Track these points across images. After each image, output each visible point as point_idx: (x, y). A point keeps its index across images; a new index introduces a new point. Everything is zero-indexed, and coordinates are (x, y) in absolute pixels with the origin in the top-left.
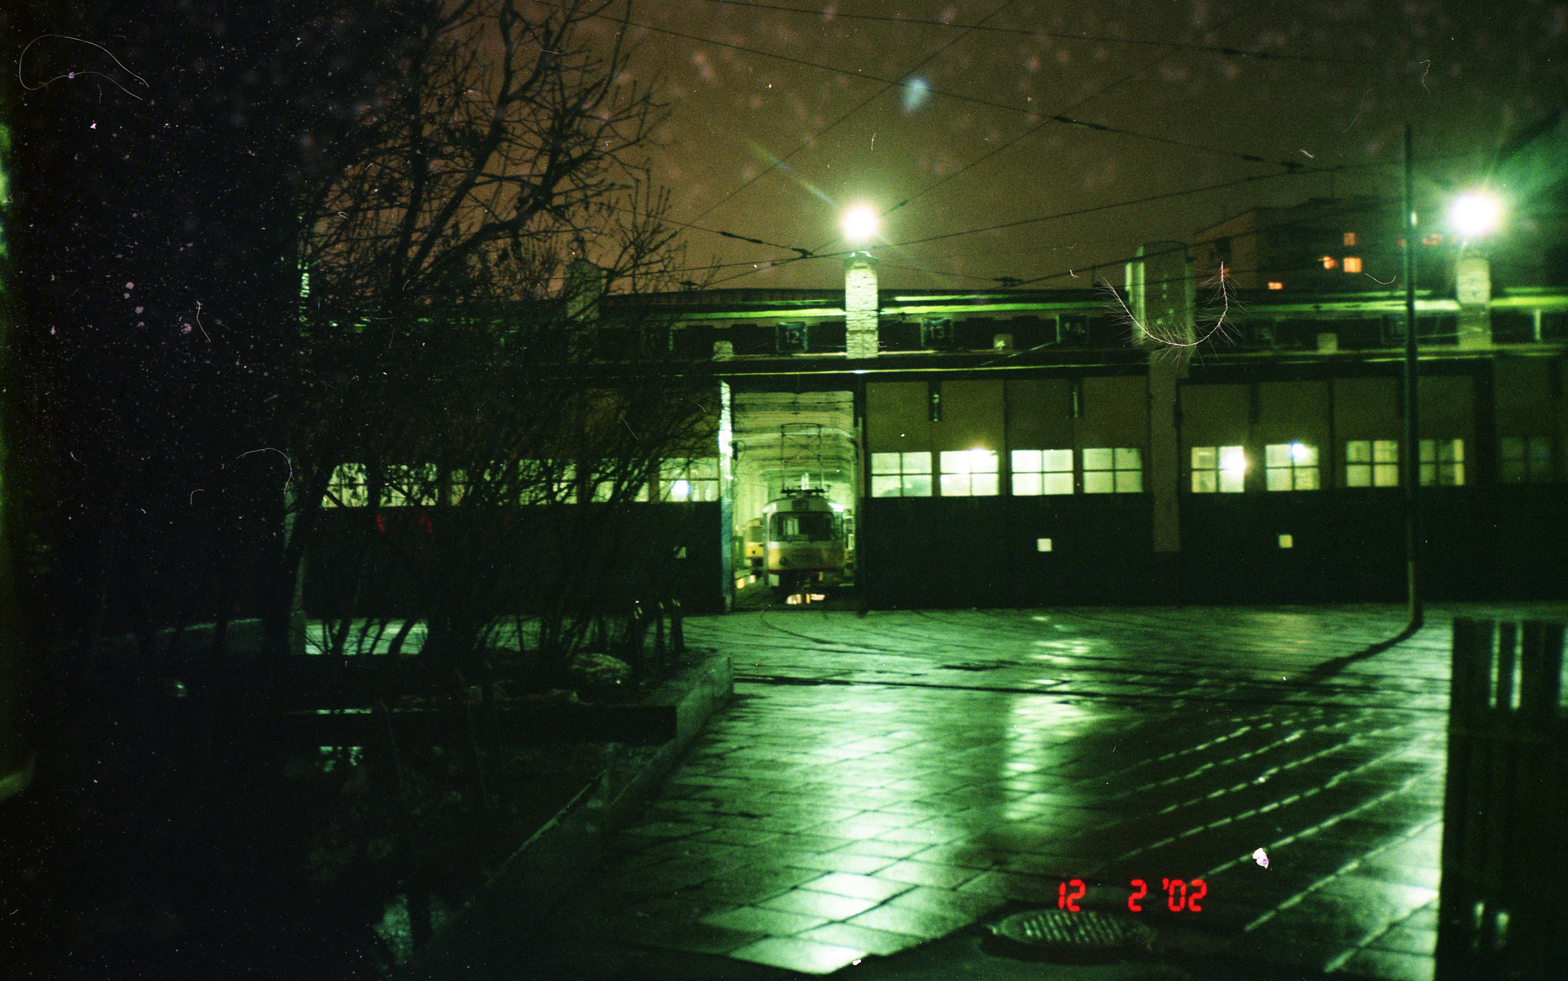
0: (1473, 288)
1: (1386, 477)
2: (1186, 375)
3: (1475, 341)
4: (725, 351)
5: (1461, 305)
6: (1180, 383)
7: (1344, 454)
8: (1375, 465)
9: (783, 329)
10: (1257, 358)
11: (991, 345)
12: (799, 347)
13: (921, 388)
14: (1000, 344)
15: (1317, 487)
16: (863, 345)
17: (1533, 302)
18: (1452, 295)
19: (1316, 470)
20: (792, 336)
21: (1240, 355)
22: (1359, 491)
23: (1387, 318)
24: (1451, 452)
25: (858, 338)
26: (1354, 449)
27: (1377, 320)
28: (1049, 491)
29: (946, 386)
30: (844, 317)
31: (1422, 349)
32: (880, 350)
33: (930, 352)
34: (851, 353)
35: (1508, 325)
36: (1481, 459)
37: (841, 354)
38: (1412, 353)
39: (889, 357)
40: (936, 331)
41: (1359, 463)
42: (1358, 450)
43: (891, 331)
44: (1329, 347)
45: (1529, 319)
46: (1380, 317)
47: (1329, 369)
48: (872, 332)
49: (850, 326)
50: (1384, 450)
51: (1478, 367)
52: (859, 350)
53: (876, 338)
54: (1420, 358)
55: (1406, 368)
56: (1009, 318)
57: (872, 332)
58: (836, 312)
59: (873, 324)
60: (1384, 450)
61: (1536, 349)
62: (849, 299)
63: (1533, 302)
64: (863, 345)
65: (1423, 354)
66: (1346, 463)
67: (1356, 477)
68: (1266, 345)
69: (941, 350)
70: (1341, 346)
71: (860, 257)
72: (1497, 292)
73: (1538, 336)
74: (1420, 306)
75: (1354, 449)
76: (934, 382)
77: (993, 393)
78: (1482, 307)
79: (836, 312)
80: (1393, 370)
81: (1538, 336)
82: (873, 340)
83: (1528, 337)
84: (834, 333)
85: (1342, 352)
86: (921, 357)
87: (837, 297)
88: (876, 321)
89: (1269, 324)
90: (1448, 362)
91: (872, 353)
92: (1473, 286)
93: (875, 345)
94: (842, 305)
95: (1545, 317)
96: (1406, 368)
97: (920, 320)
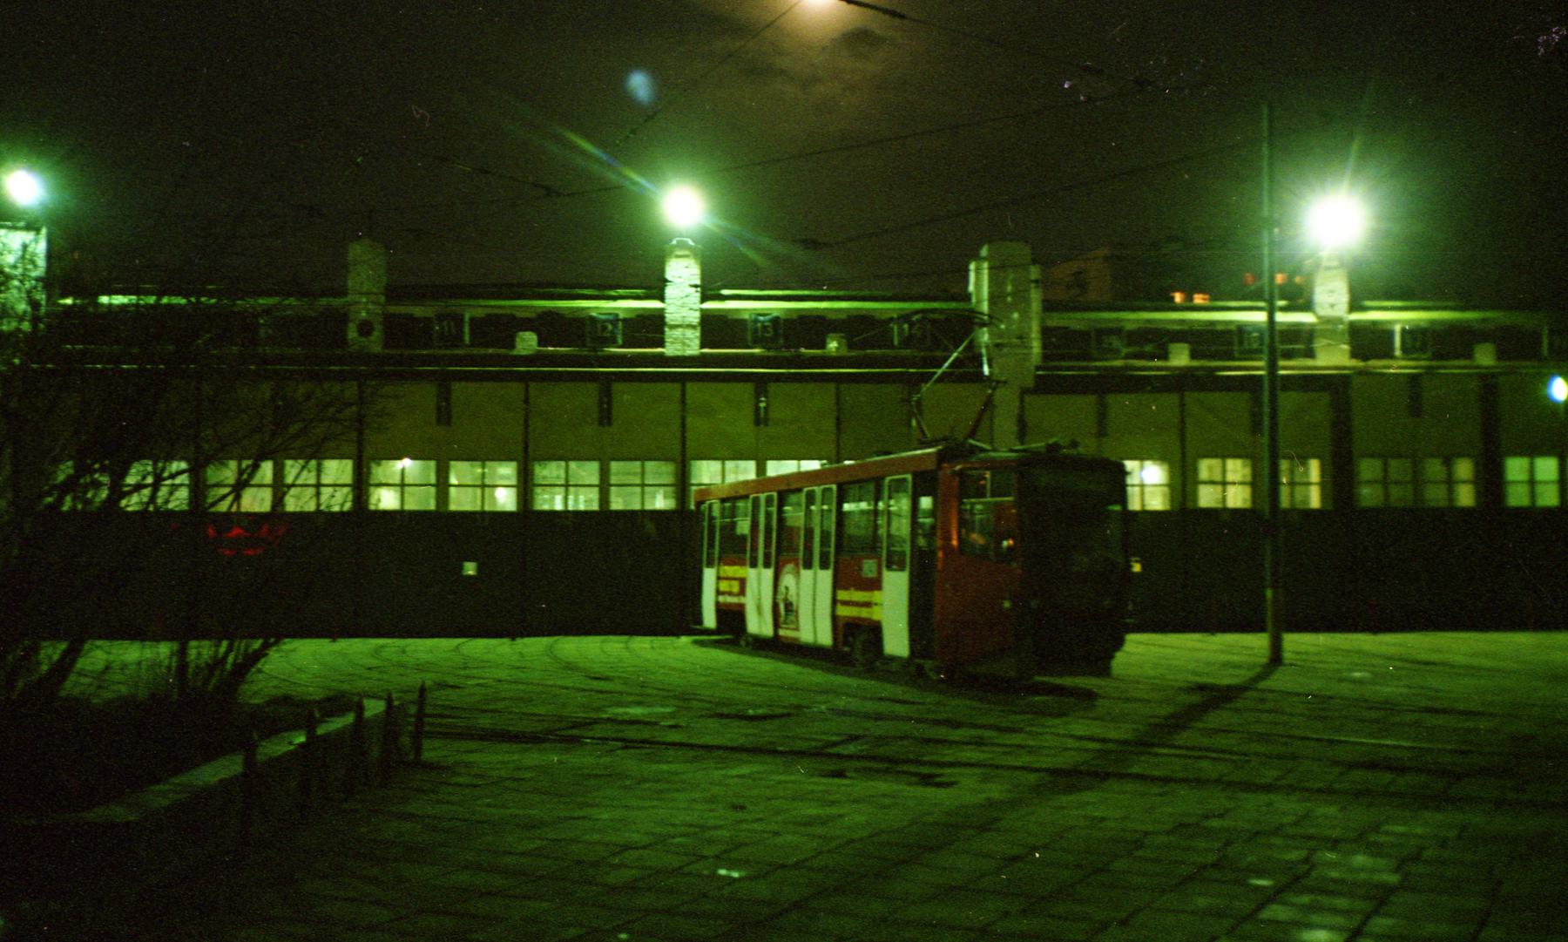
0: (1331, 300)
1: (1238, 498)
2: (1030, 383)
3: (1333, 357)
4: (527, 342)
5: (1319, 317)
6: (1024, 392)
7: (1195, 471)
8: (1228, 485)
9: (592, 319)
10: (1106, 369)
11: (823, 345)
12: (612, 342)
13: (749, 387)
14: (833, 345)
15: (1167, 507)
16: (683, 342)
17: (1398, 318)
18: (1308, 307)
19: (1166, 489)
20: (604, 328)
21: (862, 353)
22: (1210, 513)
23: (1241, 330)
24: (1307, 473)
25: (678, 332)
26: (1207, 468)
27: (1229, 332)
28: (1129, 489)
29: (773, 388)
30: (662, 310)
31: (1281, 363)
32: (703, 346)
33: (756, 351)
34: (669, 350)
35: (1368, 341)
36: (1340, 480)
37: (659, 350)
38: (1272, 367)
39: (711, 355)
40: (764, 327)
41: (1213, 483)
42: (1210, 468)
43: (715, 328)
44: (1180, 358)
45: (1391, 334)
46: (1233, 327)
47: (1181, 382)
48: (694, 327)
49: (669, 318)
50: (1237, 469)
51: (1334, 385)
52: (679, 346)
53: (698, 333)
54: (1282, 372)
55: (1266, 383)
56: (843, 316)
57: (694, 327)
58: (653, 304)
59: (695, 318)
60: (1237, 469)
61: (1398, 365)
62: (669, 291)
63: (1398, 318)
64: (683, 342)
65: (1285, 368)
66: (1197, 482)
67: (1207, 497)
68: (1115, 353)
69: (769, 349)
70: (1193, 356)
71: (682, 245)
72: (1355, 306)
73: (1398, 353)
74: (1281, 317)
75: (1207, 468)
76: (761, 383)
77: (822, 399)
78: (1340, 320)
79: (653, 304)
80: (1252, 384)
81: (1398, 353)
82: (694, 336)
83: (1388, 354)
84: (651, 327)
85: (1196, 363)
86: (737, 356)
87: (656, 287)
88: (698, 314)
89: (1118, 331)
90: (1305, 377)
91: (694, 349)
92: (1331, 298)
93: (697, 342)
94: (662, 298)
95: (1404, 331)
96: (1266, 383)
97: (746, 316)
